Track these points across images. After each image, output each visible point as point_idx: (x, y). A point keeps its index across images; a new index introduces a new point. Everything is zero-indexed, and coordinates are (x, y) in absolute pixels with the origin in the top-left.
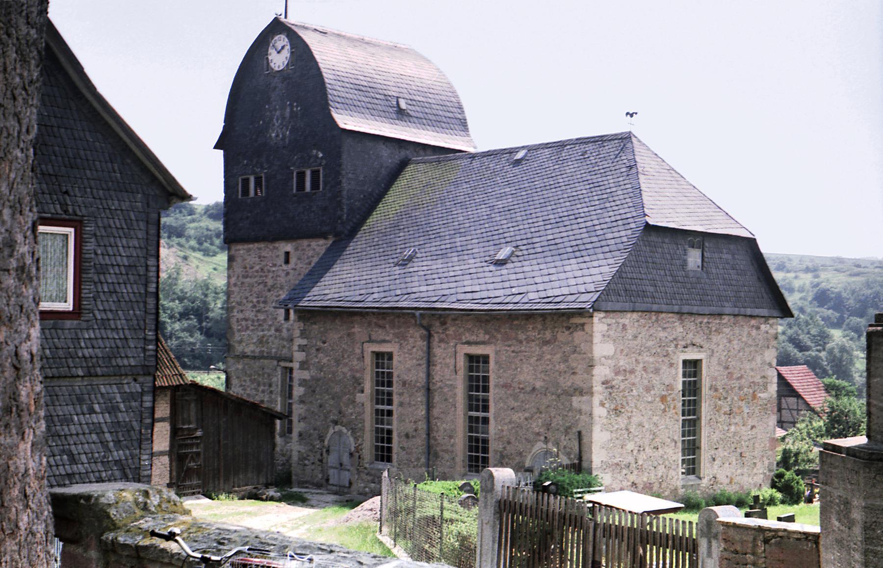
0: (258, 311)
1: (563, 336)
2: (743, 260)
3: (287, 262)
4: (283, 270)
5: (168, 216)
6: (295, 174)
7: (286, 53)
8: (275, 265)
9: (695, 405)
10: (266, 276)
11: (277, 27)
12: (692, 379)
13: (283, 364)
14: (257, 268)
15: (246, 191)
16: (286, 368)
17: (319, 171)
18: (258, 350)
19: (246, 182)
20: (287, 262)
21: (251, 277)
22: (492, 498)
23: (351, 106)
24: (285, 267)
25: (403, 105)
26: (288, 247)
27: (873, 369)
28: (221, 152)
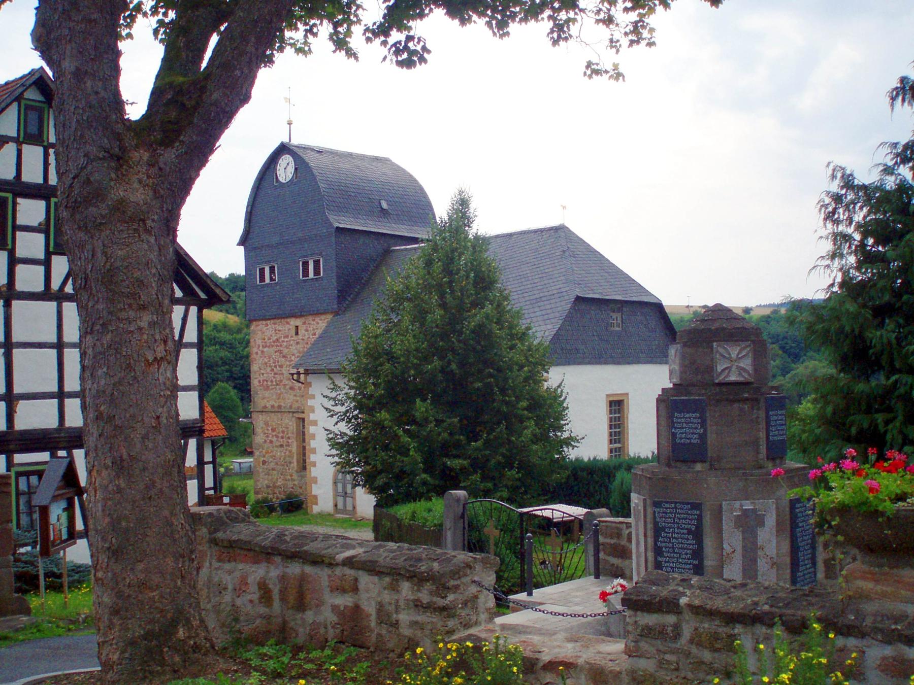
0: (275, 374)
1: (831, 617)
2: (654, 322)
3: (297, 333)
4: (294, 340)
5: (235, 322)
6: (301, 263)
7: (291, 169)
8: (287, 337)
9: (619, 435)
10: (281, 346)
11: (283, 149)
12: (617, 415)
13: (297, 415)
14: (275, 338)
15: (262, 278)
16: (299, 418)
17: (319, 260)
18: (276, 405)
19: (262, 271)
20: (297, 333)
21: (269, 347)
22: (216, 350)
23: (341, 209)
24: (295, 338)
25: (384, 205)
26: (298, 322)
27: (646, 310)
28: (242, 248)
